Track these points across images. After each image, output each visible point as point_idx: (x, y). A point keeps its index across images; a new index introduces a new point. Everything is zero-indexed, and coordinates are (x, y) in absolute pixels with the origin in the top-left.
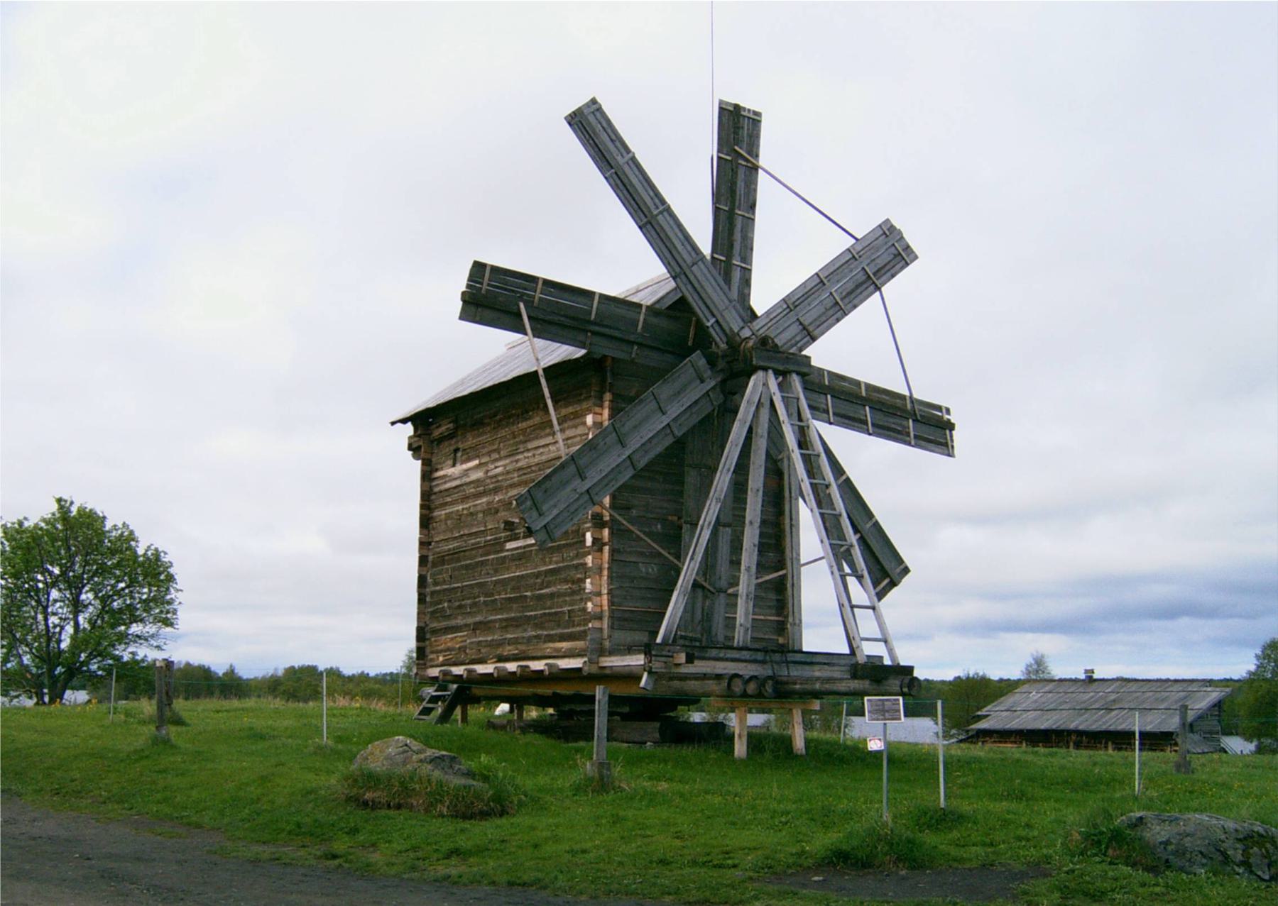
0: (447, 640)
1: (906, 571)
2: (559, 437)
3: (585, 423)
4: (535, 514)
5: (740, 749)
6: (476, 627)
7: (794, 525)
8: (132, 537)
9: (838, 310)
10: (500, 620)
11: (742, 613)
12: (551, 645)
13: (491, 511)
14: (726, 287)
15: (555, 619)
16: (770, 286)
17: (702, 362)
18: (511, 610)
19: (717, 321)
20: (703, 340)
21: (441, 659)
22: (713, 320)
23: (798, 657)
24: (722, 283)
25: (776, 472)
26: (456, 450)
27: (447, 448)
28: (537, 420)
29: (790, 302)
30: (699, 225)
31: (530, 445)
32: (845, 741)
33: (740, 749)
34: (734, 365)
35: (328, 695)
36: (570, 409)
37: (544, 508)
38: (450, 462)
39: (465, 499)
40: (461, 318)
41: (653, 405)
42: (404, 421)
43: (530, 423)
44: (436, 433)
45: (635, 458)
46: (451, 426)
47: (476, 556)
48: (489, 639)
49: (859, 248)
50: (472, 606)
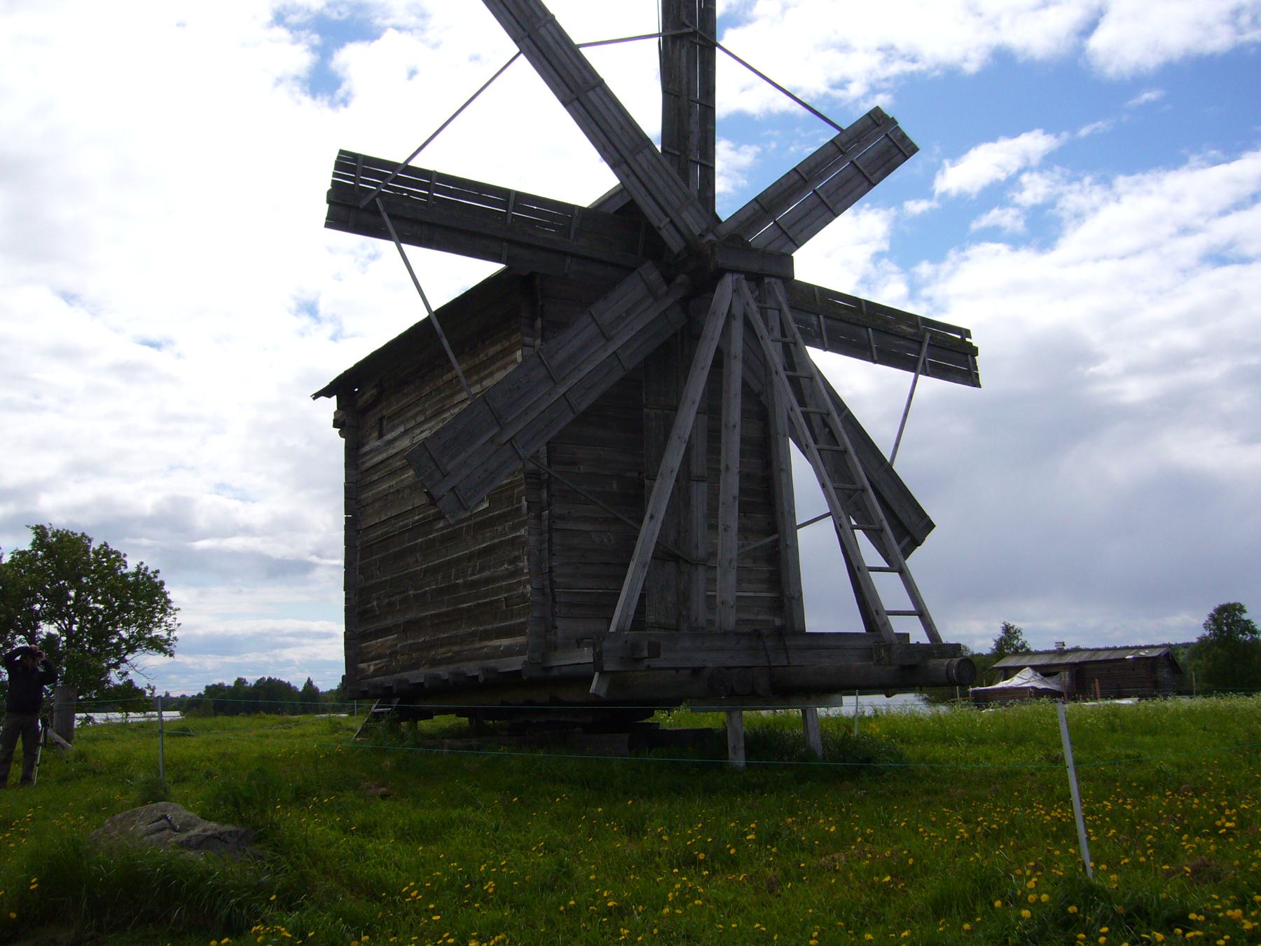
1: (930, 526)
3: (515, 361)
5: (738, 759)
6: (408, 628)
7: (786, 468)
8: (119, 558)
9: (827, 210)
11: (727, 586)
12: (487, 643)
14: (683, 185)
16: (736, 177)
17: (654, 276)
19: (672, 222)
20: (654, 247)
21: (372, 668)
24: (678, 178)
25: (759, 410)
26: (381, 420)
30: (645, 107)
33: (738, 759)
35: (68, 740)
36: (498, 347)
38: (376, 434)
39: (392, 474)
40: (328, 225)
42: (326, 392)
44: (361, 402)
48: (421, 640)
49: (845, 139)
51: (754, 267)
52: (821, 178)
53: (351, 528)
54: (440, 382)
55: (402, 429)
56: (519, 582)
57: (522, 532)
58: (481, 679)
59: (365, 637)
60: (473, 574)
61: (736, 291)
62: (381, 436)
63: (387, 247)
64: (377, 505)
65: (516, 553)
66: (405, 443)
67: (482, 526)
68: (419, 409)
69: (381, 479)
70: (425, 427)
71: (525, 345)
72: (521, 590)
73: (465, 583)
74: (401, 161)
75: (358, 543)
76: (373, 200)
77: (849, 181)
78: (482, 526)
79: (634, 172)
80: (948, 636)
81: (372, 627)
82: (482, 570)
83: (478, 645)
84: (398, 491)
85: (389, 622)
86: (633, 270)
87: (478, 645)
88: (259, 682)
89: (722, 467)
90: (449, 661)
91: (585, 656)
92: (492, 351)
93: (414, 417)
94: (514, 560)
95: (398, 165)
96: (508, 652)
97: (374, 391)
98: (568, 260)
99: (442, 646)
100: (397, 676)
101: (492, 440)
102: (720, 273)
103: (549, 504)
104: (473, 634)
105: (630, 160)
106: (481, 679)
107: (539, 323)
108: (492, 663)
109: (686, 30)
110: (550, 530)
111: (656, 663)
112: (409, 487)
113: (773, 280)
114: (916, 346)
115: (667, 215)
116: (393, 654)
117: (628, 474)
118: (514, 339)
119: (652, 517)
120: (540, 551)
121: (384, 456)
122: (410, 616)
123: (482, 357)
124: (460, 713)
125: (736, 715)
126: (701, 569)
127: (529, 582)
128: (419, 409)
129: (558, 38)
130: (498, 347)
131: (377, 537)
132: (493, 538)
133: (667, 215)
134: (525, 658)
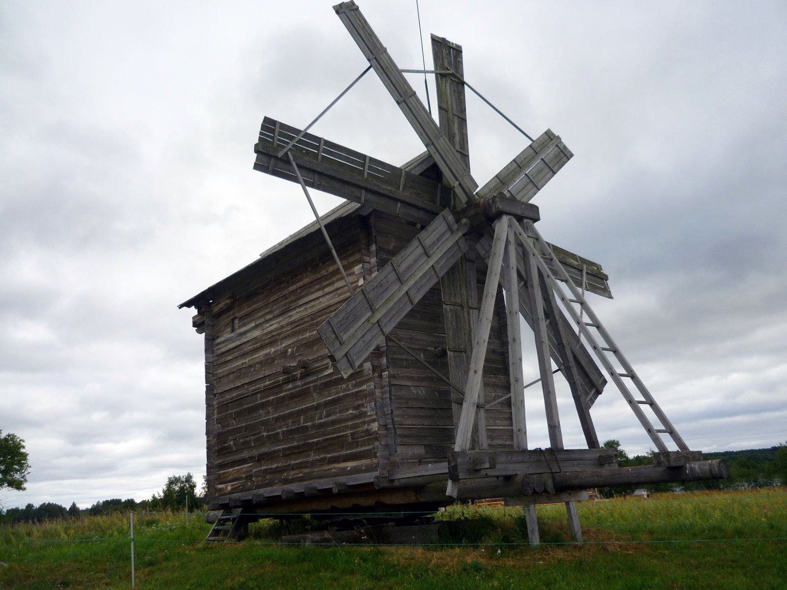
4: (337, 344)
5: (535, 540)
6: (261, 458)
13: (269, 361)
15: (340, 442)
17: (451, 218)
21: (229, 488)
22: (458, 183)
23: (565, 456)
26: (233, 320)
27: (225, 319)
28: (331, 269)
29: (519, 162)
31: (301, 302)
33: (535, 540)
37: (345, 338)
38: (229, 329)
39: (244, 355)
41: (420, 250)
42: (188, 304)
43: (300, 284)
44: (216, 309)
45: (412, 294)
46: (228, 301)
48: (274, 466)
50: (256, 441)
51: (519, 212)
53: (210, 391)
54: (286, 292)
55: (253, 324)
56: (364, 423)
59: (222, 466)
60: (321, 418)
61: (510, 226)
62: (233, 331)
63: (297, 187)
65: (360, 402)
66: (256, 333)
69: (235, 358)
70: (274, 322)
72: (366, 427)
75: (215, 403)
76: (286, 153)
77: (542, 170)
79: (438, 151)
80: (693, 446)
81: (230, 459)
84: (250, 366)
85: (245, 454)
86: (437, 214)
88: (41, 506)
90: (300, 480)
92: (306, 280)
95: (300, 131)
97: (228, 301)
101: (368, 320)
102: (499, 214)
104: (322, 460)
105: (435, 143)
108: (342, 479)
109: (448, 72)
110: (390, 385)
113: (529, 220)
114: (579, 273)
115: (457, 179)
116: (249, 477)
117: (429, 348)
118: (357, 256)
119: (475, 372)
121: (238, 343)
123: (324, 273)
124: (275, 517)
133: (457, 179)
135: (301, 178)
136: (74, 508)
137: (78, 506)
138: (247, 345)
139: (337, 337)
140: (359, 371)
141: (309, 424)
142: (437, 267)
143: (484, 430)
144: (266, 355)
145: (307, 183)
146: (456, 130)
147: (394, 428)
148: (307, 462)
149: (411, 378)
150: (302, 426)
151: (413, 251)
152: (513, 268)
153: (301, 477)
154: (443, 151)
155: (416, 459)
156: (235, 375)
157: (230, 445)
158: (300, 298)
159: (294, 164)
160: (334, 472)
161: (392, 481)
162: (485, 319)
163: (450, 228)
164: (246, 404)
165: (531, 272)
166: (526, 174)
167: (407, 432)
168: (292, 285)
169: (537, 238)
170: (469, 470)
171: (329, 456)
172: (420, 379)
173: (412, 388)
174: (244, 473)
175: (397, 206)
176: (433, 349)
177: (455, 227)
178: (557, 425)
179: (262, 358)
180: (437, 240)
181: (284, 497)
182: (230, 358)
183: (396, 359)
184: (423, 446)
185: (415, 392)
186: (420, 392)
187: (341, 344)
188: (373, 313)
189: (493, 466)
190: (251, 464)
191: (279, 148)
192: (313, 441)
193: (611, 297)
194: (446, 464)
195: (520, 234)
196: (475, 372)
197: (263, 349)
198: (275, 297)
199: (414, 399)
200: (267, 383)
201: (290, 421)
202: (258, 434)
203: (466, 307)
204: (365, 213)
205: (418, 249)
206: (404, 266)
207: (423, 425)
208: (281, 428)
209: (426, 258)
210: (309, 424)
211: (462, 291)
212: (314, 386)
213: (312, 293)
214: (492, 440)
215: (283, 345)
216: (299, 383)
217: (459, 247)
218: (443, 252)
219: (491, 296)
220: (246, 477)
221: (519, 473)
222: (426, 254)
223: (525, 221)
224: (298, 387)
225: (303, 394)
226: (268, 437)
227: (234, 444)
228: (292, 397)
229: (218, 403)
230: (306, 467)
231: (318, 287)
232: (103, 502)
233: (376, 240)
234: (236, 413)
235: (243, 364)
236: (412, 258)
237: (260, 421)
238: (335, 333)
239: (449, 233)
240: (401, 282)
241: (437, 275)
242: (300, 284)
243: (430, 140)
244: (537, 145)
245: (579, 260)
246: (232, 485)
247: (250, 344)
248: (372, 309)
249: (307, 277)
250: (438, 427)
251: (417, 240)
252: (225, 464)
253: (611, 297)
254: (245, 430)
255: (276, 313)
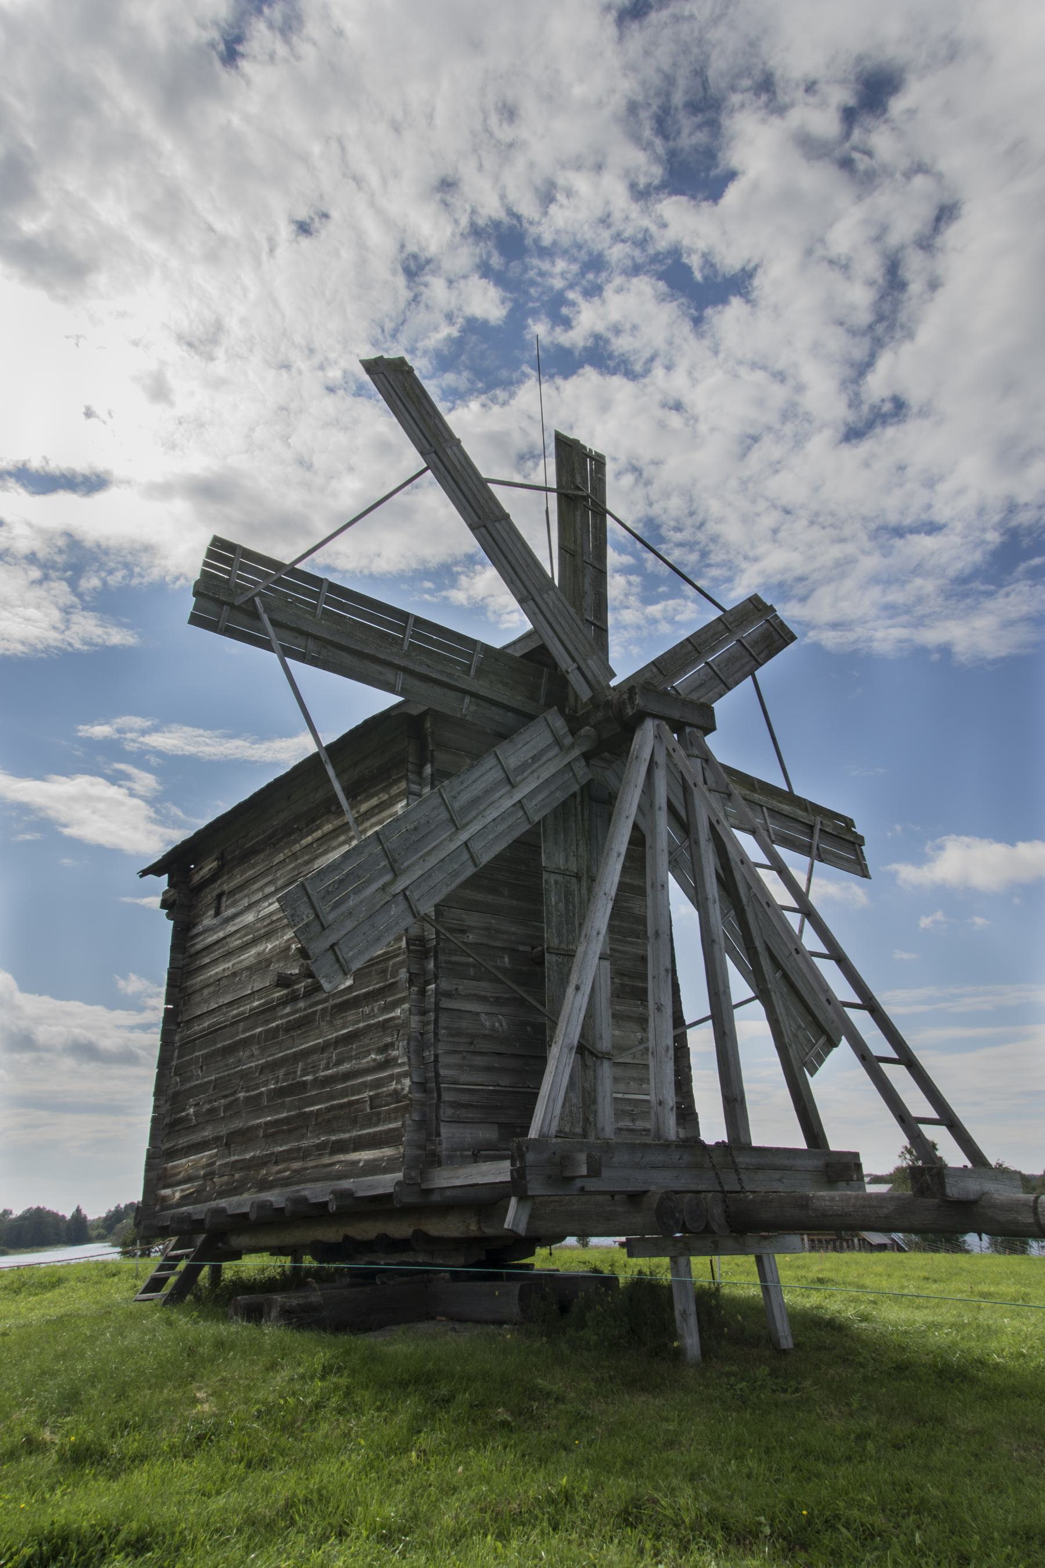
0: (184, 1164)
2: (349, 817)
10: (267, 1124)
12: (342, 1157)
13: (262, 965)
15: (350, 1115)
17: (560, 724)
18: (282, 1107)
19: (579, 668)
21: (178, 1195)
22: (575, 665)
26: (220, 896)
32: (802, 1234)
34: (610, 723)
36: (374, 801)
38: (212, 912)
42: (156, 869)
43: (319, 834)
44: (197, 878)
47: (237, 1034)
48: (248, 1156)
50: (227, 1108)
51: (676, 715)
52: (713, 650)
56: (391, 1077)
57: (398, 1012)
58: (333, 1207)
59: (172, 1154)
60: (327, 1068)
61: (658, 737)
62: (217, 913)
63: (272, 658)
64: (206, 992)
65: (389, 1040)
67: (344, 1007)
68: (270, 878)
69: (215, 962)
71: (411, 793)
72: (393, 1085)
73: (315, 1079)
74: (287, 562)
75: (177, 1038)
78: (344, 1007)
79: (541, 612)
82: (339, 1063)
83: (326, 1160)
84: (234, 974)
85: (208, 1133)
86: (532, 718)
87: (326, 1160)
89: (650, 932)
90: (286, 1183)
91: (496, 1172)
92: (328, 828)
93: (261, 889)
94: (384, 1049)
96: (374, 1169)
97: (214, 864)
98: (467, 700)
99: (276, 1163)
100: (213, 1204)
101: (384, 888)
102: (641, 716)
103: (436, 977)
106: (333, 1207)
107: (428, 770)
108: (346, 1184)
109: (580, 493)
110: (437, 1009)
111: (592, 1185)
112: (248, 968)
116: (209, 1176)
117: (521, 948)
118: (403, 785)
119: (578, 988)
120: (422, 1034)
121: (221, 934)
122: (238, 1124)
124: (277, 1251)
125: (682, 1260)
126: (606, 1064)
127: (405, 1075)
128: (270, 878)
129: (465, 464)
130: (374, 801)
131: (203, 1030)
132: (358, 1022)
133: (574, 660)
134: (399, 1176)
135: (276, 643)
136: (79, 1218)
137: (84, 1212)
138: (233, 939)
139: (317, 916)
140: (392, 984)
141: (309, 1078)
142: (530, 806)
143: (608, 1099)
144: (259, 954)
145: (287, 652)
146: (587, 586)
147: (439, 1089)
148: (299, 1149)
149: (484, 999)
150: (298, 1082)
151: (485, 775)
152: (660, 808)
153: (288, 1178)
154: (553, 613)
155: (469, 1150)
156: (211, 989)
157: (188, 1115)
158: (316, 858)
159: (265, 617)
160: (338, 1171)
161: (430, 1191)
162: (602, 894)
163: (557, 742)
164: (221, 1041)
165: (695, 816)
166: (707, 663)
167: (465, 1098)
168: (307, 836)
169: (707, 758)
170: (550, 1177)
171: (334, 1138)
172: (498, 1001)
173: (483, 1017)
174: (203, 1168)
175: (463, 701)
176: (528, 949)
177: (569, 740)
178: (739, 1099)
179: (253, 961)
180: (532, 758)
181: (253, 1216)
182: (207, 960)
183: (455, 963)
184: (496, 1126)
185: (488, 1023)
186: (497, 1024)
187: (323, 928)
188: (396, 876)
189: (594, 1171)
190: (215, 1151)
191: (239, 591)
192: (312, 1109)
193: (865, 874)
194: (506, 1164)
195: (674, 750)
196: (578, 988)
197: (256, 945)
198: (281, 857)
199: (485, 1036)
200: (256, 1004)
201: (281, 1073)
202: (232, 1095)
203: (585, 878)
204: (415, 711)
205: (493, 771)
206: (465, 797)
207: (499, 1085)
208: (266, 1085)
209: (508, 788)
210: (309, 1078)
211: (580, 849)
212: (322, 1009)
213: (334, 849)
214: (633, 1120)
215: (285, 938)
216: (301, 1004)
217: (574, 774)
218: (541, 780)
219: (615, 855)
220: (205, 1175)
221: (653, 1188)
222: (510, 782)
223: (688, 730)
224: (300, 1010)
225: (303, 1024)
226: (247, 1099)
227: (196, 1114)
228: (289, 1028)
229: (182, 1039)
230: (295, 1159)
231: (342, 838)
232: (126, 1206)
233: (432, 756)
234: (206, 1057)
235: (224, 970)
236: (481, 786)
237: (238, 1072)
238: (313, 907)
239: (556, 750)
240: (455, 825)
241: (528, 819)
242: (319, 834)
243: (529, 592)
244: (731, 619)
245: (757, 786)
246: (182, 1190)
247: (238, 935)
248: (393, 870)
249: (328, 821)
250: (528, 1090)
251: (493, 756)
252: (177, 1150)
253: (865, 874)
254: (214, 1088)
255: (280, 883)
